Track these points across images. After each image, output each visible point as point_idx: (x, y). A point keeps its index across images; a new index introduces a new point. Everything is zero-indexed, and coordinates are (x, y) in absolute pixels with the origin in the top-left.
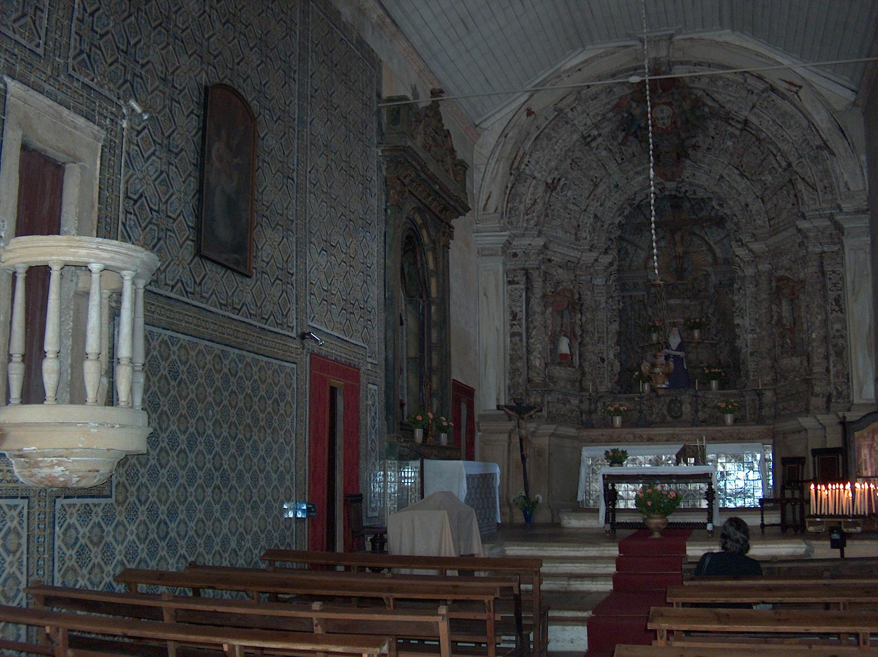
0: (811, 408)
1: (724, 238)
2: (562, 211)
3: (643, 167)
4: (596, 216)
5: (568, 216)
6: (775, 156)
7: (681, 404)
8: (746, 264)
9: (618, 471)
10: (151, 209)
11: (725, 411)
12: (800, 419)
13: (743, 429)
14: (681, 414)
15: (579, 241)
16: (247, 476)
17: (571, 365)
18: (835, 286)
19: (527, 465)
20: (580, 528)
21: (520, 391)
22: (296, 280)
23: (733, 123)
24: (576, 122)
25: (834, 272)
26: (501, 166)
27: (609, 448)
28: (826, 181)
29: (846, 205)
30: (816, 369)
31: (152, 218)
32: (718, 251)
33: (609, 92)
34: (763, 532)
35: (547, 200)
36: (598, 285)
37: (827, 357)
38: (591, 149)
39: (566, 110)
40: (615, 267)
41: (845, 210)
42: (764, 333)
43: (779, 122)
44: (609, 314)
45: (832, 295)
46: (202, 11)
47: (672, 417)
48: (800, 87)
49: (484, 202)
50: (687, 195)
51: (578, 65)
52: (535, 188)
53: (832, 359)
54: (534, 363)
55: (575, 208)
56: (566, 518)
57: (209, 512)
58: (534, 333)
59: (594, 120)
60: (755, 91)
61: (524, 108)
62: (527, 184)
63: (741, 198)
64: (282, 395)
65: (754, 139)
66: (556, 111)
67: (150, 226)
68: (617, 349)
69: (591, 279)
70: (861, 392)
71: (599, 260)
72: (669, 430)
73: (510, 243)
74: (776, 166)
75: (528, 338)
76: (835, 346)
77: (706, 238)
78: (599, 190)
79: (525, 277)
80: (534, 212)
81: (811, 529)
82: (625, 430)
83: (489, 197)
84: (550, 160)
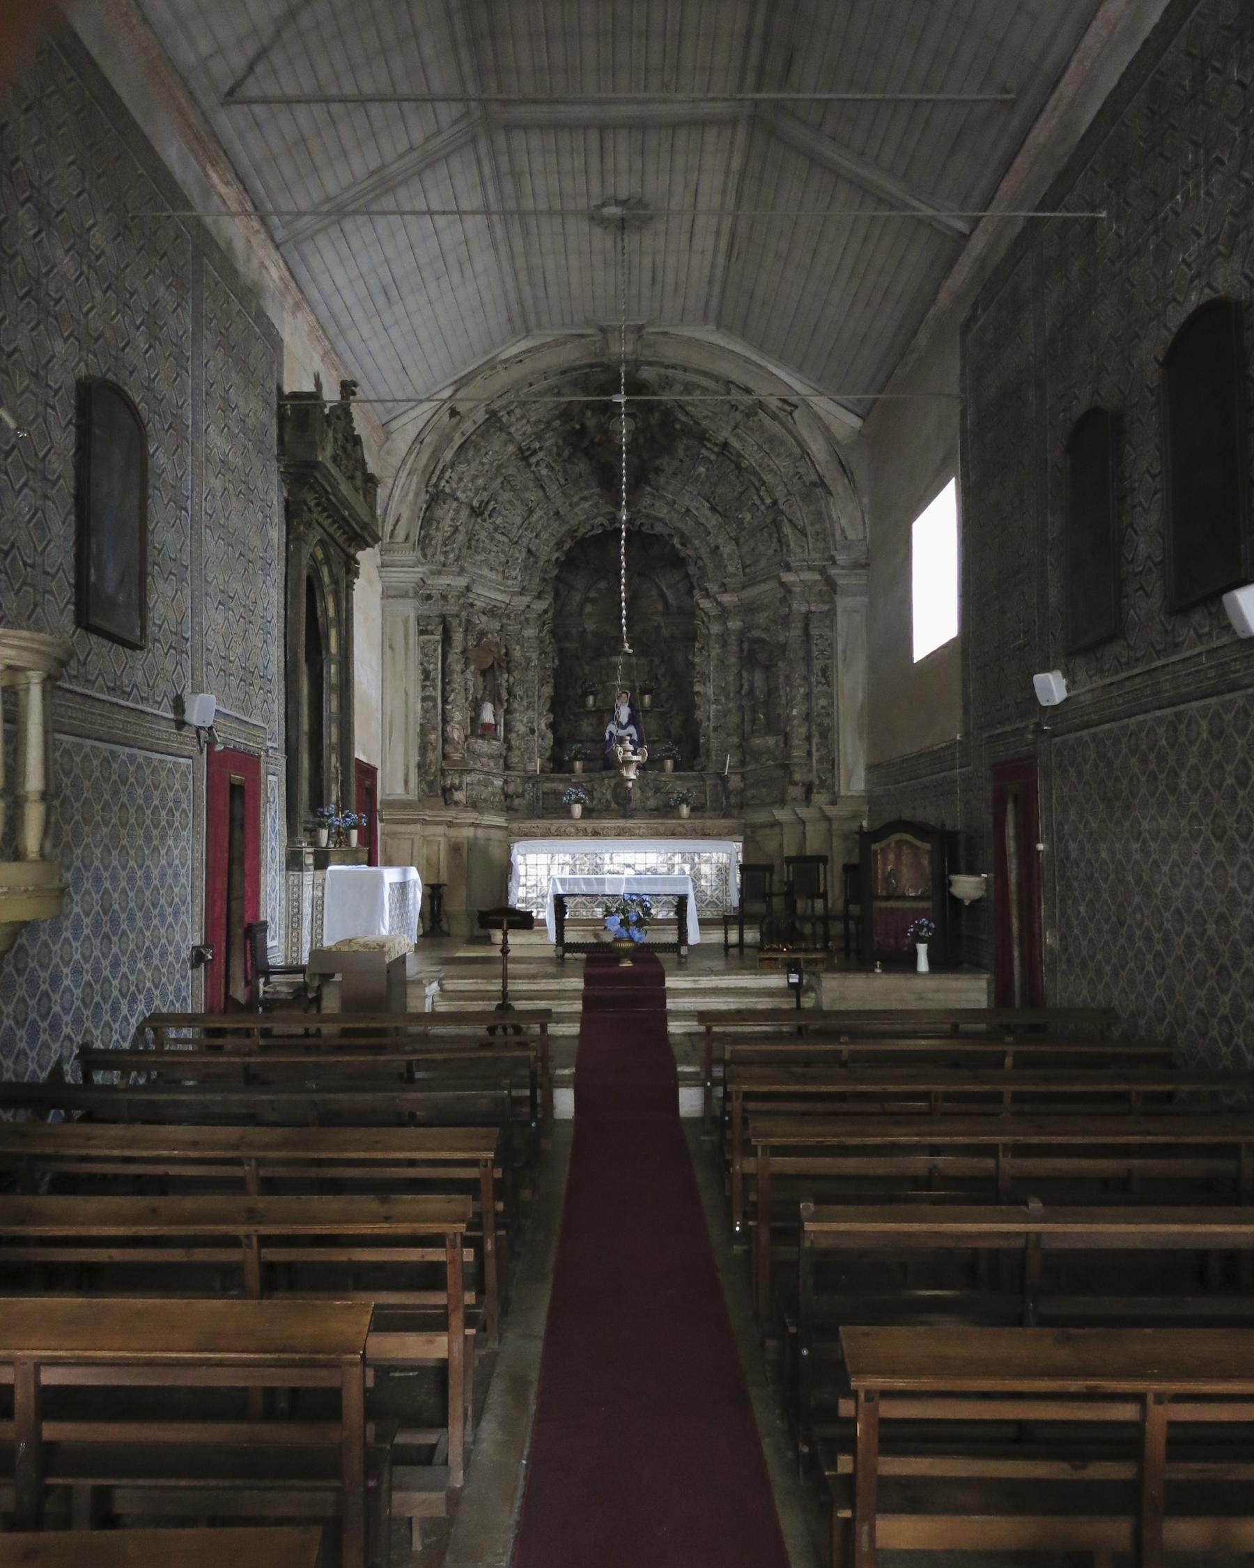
0: (788, 798)
2: (487, 541)
4: (529, 551)
5: (495, 549)
6: (758, 490)
10: (25, 564)
12: (775, 812)
16: (139, 915)
22: (192, 647)
23: (709, 445)
24: (512, 430)
25: (821, 636)
30: (795, 753)
31: (27, 576)
37: (808, 739)
38: (529, 465)
40: (550, 615)
42: (731, 705)
46: (78, 273)
47: (618, 803)
48: (796, 407)
50: (643, 529)
52: (457, 511)
53: (815, 741)
55: (505, 539)
57: (96, 970)
58: (452, 697)
60: (741, 407)
61: (447, 406)
63: (711, 539)
64: (177, 802)
65: (733, 466)
67: (25, 588)
72: (621, 823)
73: (424, 582)
74: (758, 502)
78: (534, 518)
79: (441, 627)
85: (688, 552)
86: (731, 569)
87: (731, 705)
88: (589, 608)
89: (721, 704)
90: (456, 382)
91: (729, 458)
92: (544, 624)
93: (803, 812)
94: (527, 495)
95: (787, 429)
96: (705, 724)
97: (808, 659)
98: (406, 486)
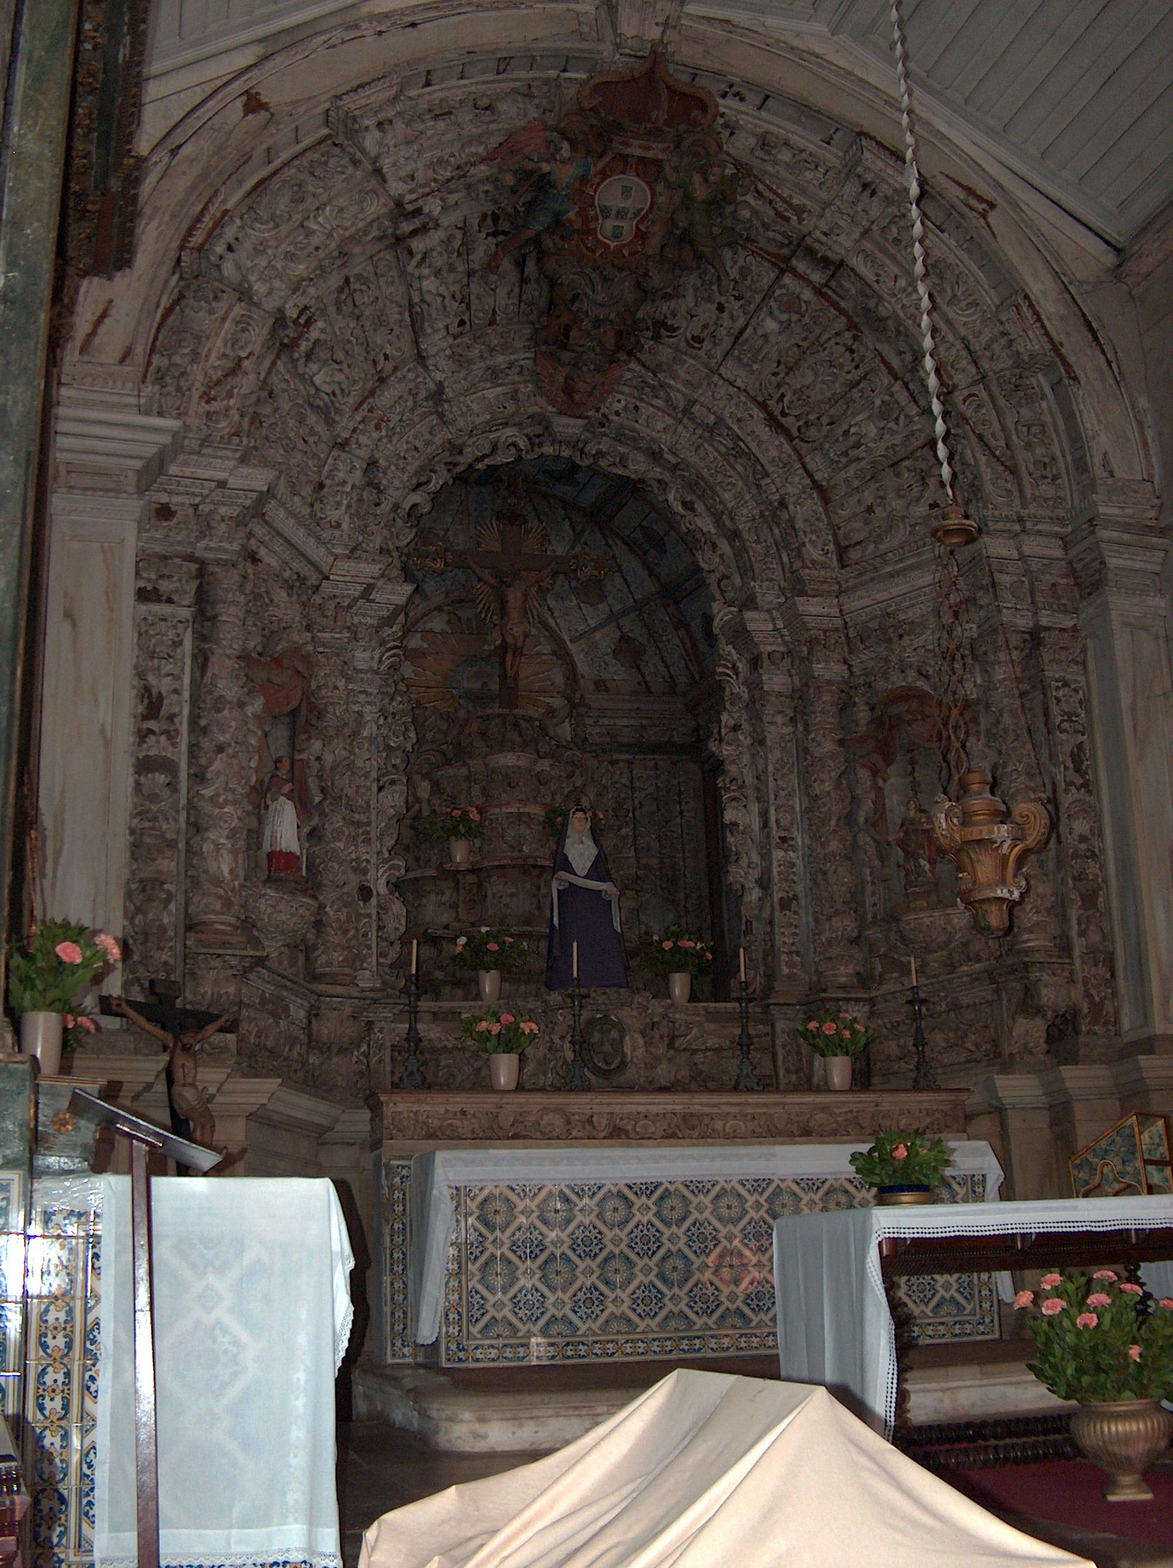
1: (595, 629)
3: (513, 357)
5: (300, 445)
12: (1000, 1081)
14: (623, 1064)
21: (164, 956)
24: (386, 164)
28: (1040, 451)
32: (579, 658)
37: (1059, 909)
39: (367, 122)
45: (1066, 742)
52: (243, 324)
53: (1074, 913)
54: (213, 867)
55: (321, 428)
56: (467, 1415)
58: (217, 766)
61: (238, 87)
62: (221, 307)
65: (842, 322)
66: (327, 123)
75: (199, 777)
77: (552, 622)
78: (388, 396)
79: (194, 585)
80: (230, 395)
82: (536, 1101)
91: (835, 305)
94: (380, 338)
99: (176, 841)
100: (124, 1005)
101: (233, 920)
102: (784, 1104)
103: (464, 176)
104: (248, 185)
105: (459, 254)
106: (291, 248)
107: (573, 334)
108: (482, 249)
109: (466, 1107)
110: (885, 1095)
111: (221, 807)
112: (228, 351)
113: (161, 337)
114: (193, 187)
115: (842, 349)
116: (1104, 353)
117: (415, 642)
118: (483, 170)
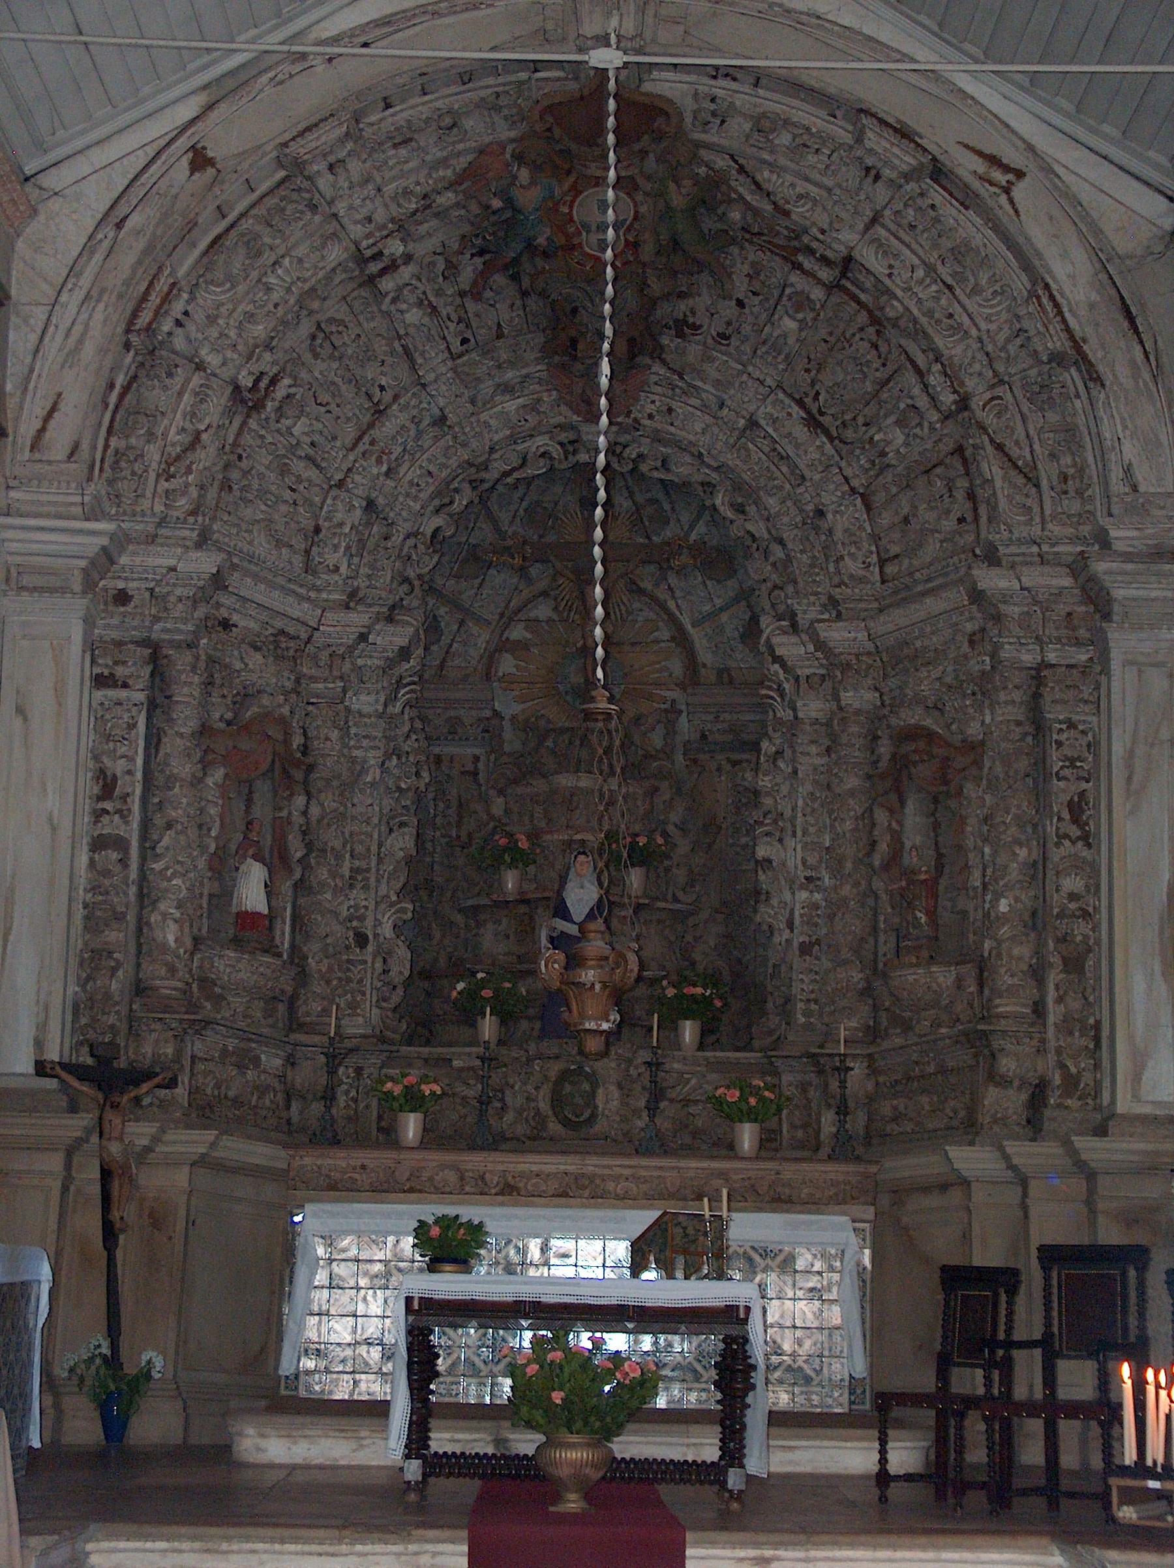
0: (984, 1119)
1: (721, 609)
3: (524, 372)
5: (287, 495)
7: (595, 1086)
8: (804, 686)
9: (453, 1287)
11: (735, 1114)
12: (954, 1152)
13: (790, 1171)
14: (593, 1116)
15: (315, 573)
17: (270, 949)
18: (1073, 766)
19: (119, 1254)
20: (294, 1467)
23: (807, 263)
24: (341, 208)
25: (1072, 725)
26: (99, 316)
27: (430, 1211)
29: (1121, 534)
30: (1005, 1006)
33: (450, 128)
34: (883, 1499)
35: (231, 440)
36: (361, 715)
37: (1037, 974)
41: (1119, 546)
43: (944, 272)
44: (388, 803)
47: (566, 1123)
48: (1020, 174)
49: (38, 425)
51: (363, 28)
52: (201, 397)
53: (1054, 977)
55: (312, 473)
56: (251, 1431)
58: (166, 841)
59: (395, 211)
60: (887, 173)
61: (183, 143)
62: (178, 380)
65: (863, 318)
66: (282, 166)
68: (403, 910)
69: (344, 691)
70: (1137, 1078)
71: (371, 638)
72: (568, 1164)
74: (922, 402)
75: (148, 849)
76: (1063, 940)
77: (671, 604)
78: (388, 427)
79: (148, 670)
80: (189, 471)
81: (1127, 1513)
82: (434, 1158)
83: (53, 409)
84: (250, 317)
85: (750, 527)
86: (852, 566)
87: (846, 890)
88: (507, 664)
89: (818, 889)
90: (205, 87)
92: (399, 683)
93: (1023, 1152)
95: (998, 229)
96: (779, 938)
97: (1040, 771)
98: (78, 329)
99: (124, 914)
100: (58, 1068)
101: (179, 985)
102: (679, 1169)
103: (429, 206)
104: (203, 245)
105: (445, 278)
106: (250, 307)
107: (580, 347)
108: (469, 269)
109: (366, 1162)
110: (786, 1165)
111: (170, 880)
112: (188, 425)
113: (118, 417)
114: (139, 262)
115: (866, 345)
116: (1141, 342)
117: (517, 633)
118: (447, 199)
